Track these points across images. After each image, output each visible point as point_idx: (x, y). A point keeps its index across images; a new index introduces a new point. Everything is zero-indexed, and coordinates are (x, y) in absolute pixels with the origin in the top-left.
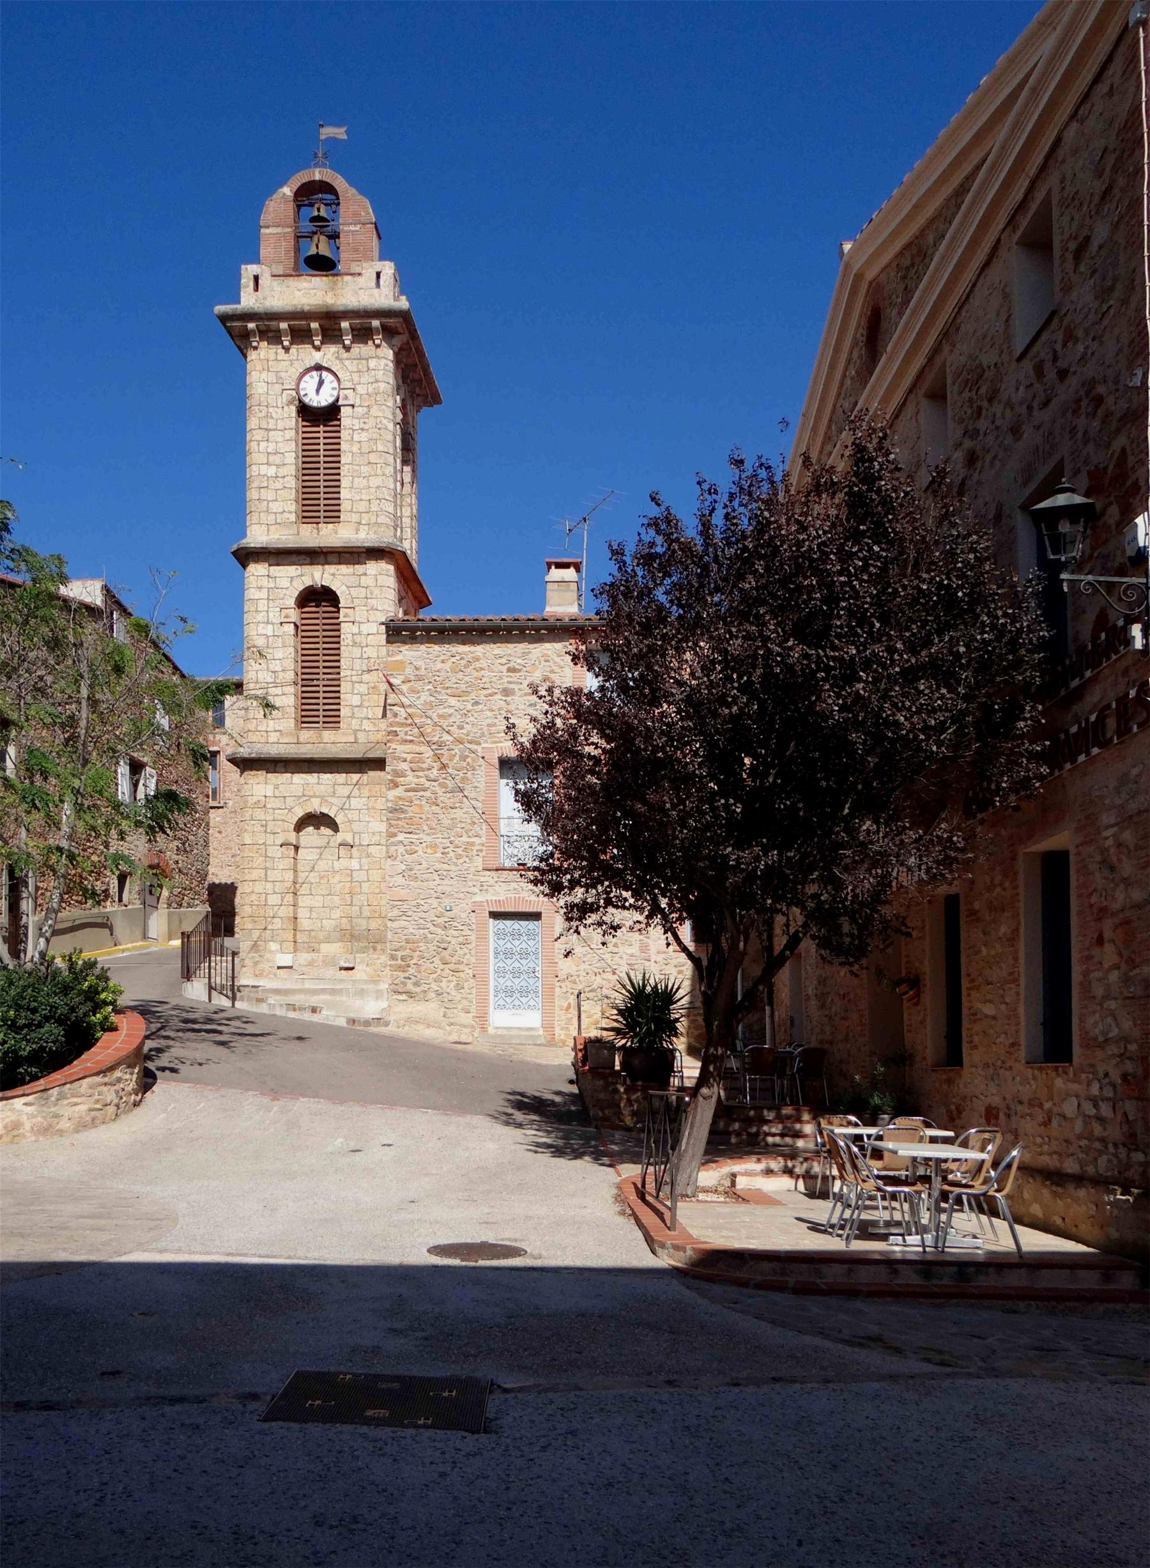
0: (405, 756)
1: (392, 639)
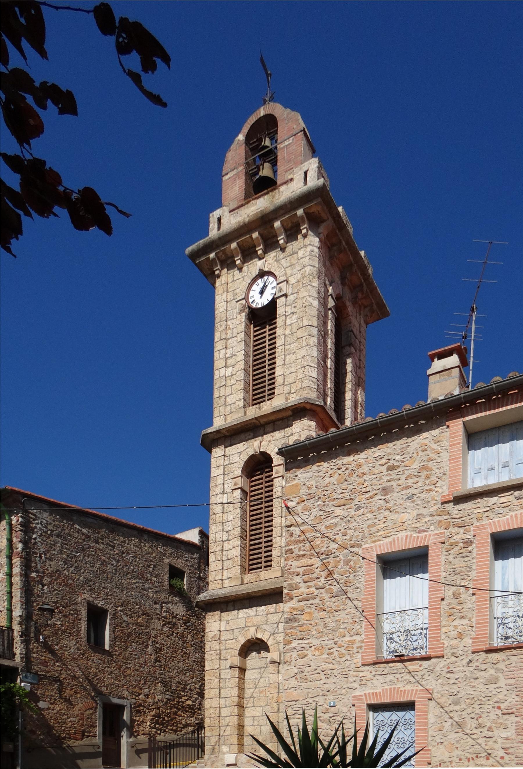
0: (298, 570)
1: (289, 467)
